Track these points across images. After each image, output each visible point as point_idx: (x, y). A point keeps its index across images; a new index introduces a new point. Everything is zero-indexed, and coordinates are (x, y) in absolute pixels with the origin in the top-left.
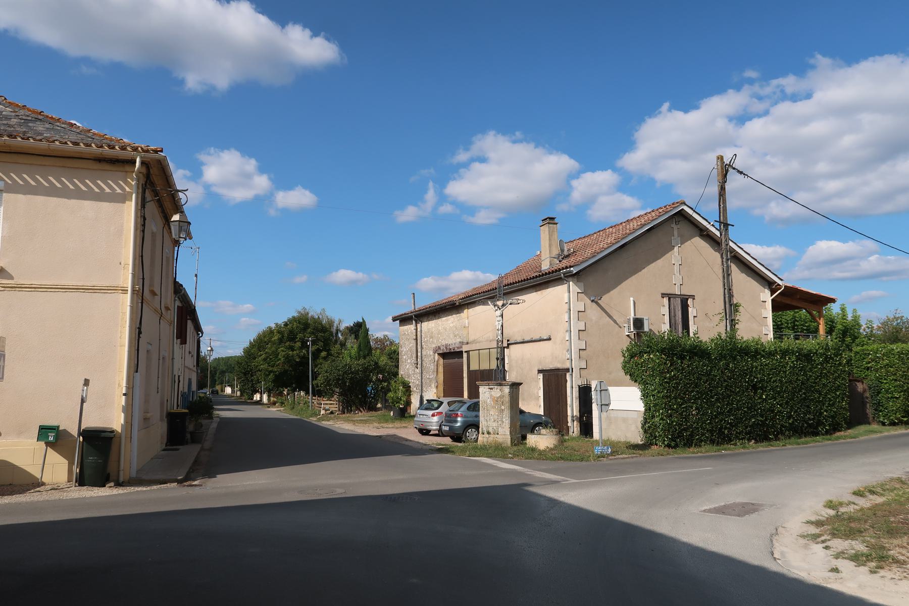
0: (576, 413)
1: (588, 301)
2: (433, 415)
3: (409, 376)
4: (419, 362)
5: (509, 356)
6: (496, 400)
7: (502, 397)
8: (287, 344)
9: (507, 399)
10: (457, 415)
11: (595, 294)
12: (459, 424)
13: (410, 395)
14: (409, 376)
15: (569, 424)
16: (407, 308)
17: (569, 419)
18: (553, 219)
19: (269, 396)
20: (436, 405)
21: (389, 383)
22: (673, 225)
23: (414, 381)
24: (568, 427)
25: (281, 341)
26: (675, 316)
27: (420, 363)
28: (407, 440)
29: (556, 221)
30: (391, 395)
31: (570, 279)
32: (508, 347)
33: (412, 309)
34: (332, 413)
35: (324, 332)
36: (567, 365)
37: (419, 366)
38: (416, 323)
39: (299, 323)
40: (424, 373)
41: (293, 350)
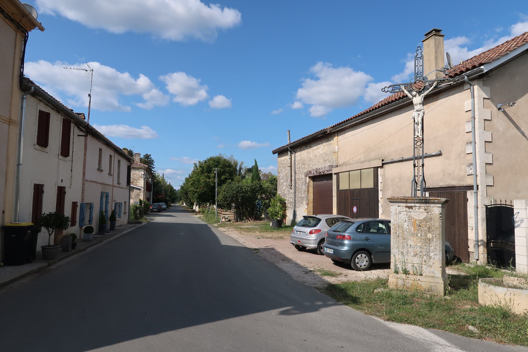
0: (482, 236)
1: (495, 109)
2: (311, 233)
3: (285, 195)
5: (383, 176)
8: (206, 174)
9: (437, 223)
11: (503, 100)
12: (346, 248)
13: (286, 210)
14: (285, 195)
15: (471, 249)
16: (285, 142)
18: (439, 31)
19: (199, 207)
21: (270, 201)
23: (289, 199)
24: (468, 253)
25: (202, 172)
27: (293, 185)
29: (441, 33)
30: (270, 209)
31: (476, 82)
32: (382, 167)
33: (288, 143)
34: (229, 221)
35: (230, 168)
36: (469, 181)
38: (291, 154)
39: (214, 161)
40: (297, 193)
41: (209, 178)
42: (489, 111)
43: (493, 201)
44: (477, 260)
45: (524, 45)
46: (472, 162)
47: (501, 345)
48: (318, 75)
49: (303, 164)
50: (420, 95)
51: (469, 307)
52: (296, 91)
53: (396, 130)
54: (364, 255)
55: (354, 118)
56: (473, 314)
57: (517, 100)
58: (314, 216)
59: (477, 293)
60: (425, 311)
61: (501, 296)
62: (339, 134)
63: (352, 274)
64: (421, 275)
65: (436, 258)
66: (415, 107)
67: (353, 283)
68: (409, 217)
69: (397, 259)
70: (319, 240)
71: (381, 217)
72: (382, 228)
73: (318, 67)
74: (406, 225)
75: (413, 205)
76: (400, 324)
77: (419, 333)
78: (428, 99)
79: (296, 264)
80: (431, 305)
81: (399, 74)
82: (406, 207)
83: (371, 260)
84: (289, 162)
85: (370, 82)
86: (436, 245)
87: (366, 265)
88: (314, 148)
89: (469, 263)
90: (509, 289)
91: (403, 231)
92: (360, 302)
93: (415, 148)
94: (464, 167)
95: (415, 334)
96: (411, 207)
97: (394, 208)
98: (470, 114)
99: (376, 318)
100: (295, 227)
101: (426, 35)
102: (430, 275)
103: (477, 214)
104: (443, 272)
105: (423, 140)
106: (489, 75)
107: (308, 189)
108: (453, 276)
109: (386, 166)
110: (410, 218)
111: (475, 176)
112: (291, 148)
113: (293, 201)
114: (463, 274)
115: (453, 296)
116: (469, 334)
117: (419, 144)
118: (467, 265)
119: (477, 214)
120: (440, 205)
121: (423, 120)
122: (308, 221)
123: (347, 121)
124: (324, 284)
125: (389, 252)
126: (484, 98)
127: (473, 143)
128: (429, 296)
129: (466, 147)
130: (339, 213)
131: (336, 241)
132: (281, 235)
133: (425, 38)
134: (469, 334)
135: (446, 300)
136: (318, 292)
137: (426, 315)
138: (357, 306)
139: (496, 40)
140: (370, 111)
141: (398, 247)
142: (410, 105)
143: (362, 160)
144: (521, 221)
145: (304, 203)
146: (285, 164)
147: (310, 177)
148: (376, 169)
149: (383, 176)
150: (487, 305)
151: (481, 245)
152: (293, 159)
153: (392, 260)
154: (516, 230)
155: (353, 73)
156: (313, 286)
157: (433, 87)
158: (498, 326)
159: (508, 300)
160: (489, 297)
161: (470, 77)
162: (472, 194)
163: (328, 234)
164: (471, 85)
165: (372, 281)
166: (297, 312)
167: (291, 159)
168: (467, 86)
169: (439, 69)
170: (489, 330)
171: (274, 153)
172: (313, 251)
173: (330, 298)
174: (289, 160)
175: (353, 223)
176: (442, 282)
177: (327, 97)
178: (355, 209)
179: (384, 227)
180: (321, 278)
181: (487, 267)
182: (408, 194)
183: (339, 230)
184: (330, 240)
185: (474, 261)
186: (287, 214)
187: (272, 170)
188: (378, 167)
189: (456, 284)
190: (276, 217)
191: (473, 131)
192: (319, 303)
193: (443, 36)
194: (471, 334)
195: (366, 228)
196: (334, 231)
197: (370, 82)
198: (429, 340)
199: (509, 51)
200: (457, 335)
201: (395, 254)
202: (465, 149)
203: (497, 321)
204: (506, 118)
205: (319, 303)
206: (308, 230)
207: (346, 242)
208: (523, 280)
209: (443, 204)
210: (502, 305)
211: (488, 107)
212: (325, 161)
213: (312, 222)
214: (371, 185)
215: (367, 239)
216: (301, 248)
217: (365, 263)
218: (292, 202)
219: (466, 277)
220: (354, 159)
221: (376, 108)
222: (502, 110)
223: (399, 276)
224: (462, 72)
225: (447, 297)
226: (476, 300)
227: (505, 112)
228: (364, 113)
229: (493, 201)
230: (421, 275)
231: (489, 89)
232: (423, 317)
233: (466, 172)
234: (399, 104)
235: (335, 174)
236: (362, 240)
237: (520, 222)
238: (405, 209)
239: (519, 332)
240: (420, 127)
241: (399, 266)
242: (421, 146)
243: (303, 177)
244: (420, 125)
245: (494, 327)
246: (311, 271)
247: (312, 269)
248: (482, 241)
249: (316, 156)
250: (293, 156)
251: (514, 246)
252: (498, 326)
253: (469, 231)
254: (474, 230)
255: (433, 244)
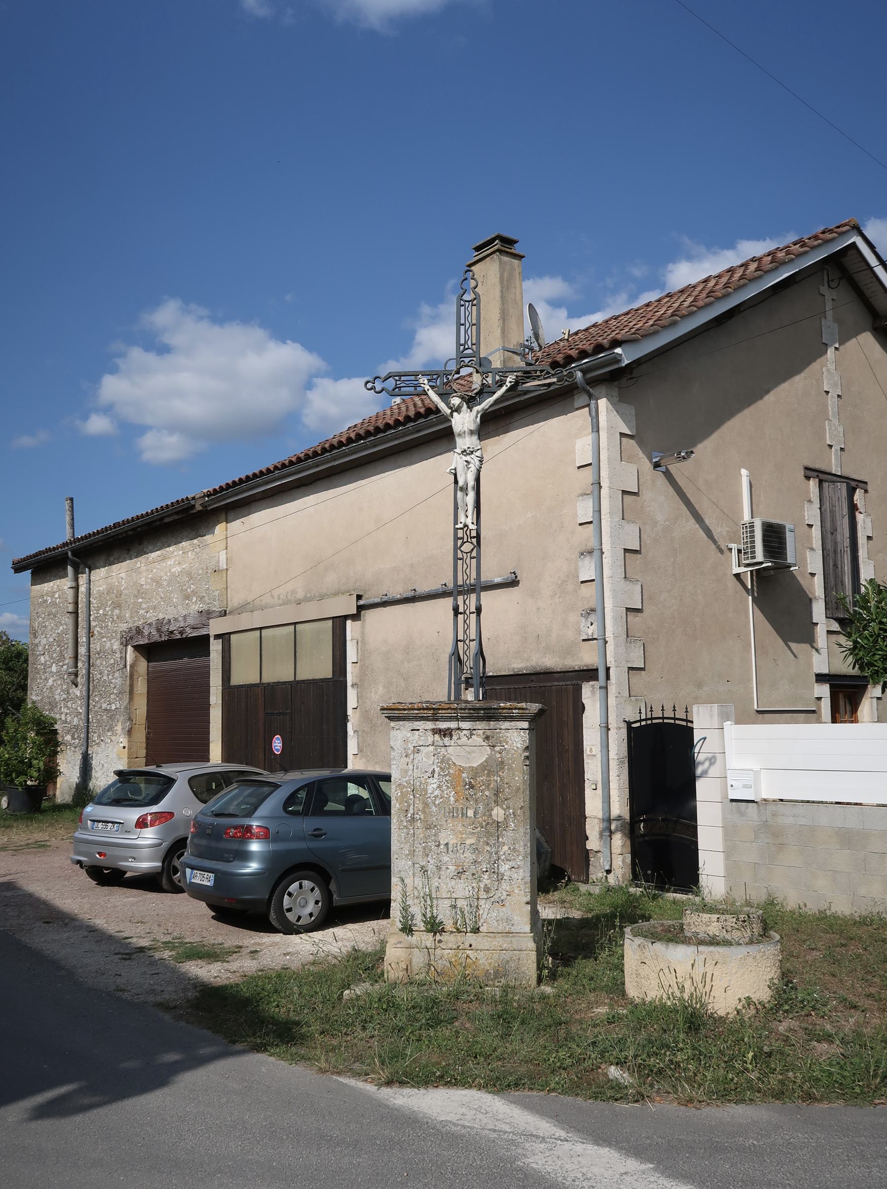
0: (620, 807)
1: (647, 466)
2: (141, 824)
3: (53, 705)
4: (81, 670)
6: (469, 784)
7: (493, 767)
9: (518, 776)
10: (247, 833)
11: (665, 440)
12: (253, 866)
13: (55, 753)
15: (593, 843)
16: (56, 535)
17: (593, 829)
18: (508, 242)
20: (153, 790)
22: (824, 289)
23: (66, 717)
24: (586, 855)
26: (834, 532)
27: (83, 671)
28: (49, 550)
29: (517, 249)
31: (602, 389)
32: (356, 617)
33: (67, 537)
36: (587, 658)
37: (81, 680)
42: (633, 469)
43: (643, 711)
44: (609, 872)
45: (710, 304)
46: (592, 604)
47: (690, 1112)
48: (167, 339)
49: (117, 605)
50: (470, 408)
51: (603, 1010)
52: (96, 380)
53: (404, 502)
54: (307, 884)
55: (276, 468)
56: (618, 1031)
57: (695, 445)
58: (152, 768)
59: (620, 968)
60: (488, 1039)
61: (683, 970)
62: (231, 515)
63: (275, 944)
64: (476, 930)
65: (515, 876)
66: (459, 441)
67: (279, 976)
68: (442, 761)
69: (409, 889)
70: (166, 845)
71: (354, 764)
72: (357, 798)
73: (166, 315)
74: (432, 785)
75: (453, 725)
76: (422, 1091)
77: (478, 1110)
78: (493, 423)
79: (93, 930)
80: (506, 1016)
81: (398, 361)
82: (435, 731)
83: (327, 895)
84: (71, 599)
85: (318, 374)
86: (515, 841)
87: (315, 914)
88: (153, 555)
89: (586, 881)
90: (702, 948)
91: (426, 805)
92: (303, 1037)
93: (456, 559)
94: (573, 617)
95: (470, 1115)
96: (446, 733)
97: (401, 735)
98: (588, 475)
99: (352, 1082)
100: (89, 809)
101: (478, 249)
102: (500, 928)
103: (606, 746)
104: (534, 913)
105: (478, 537)
106: (635, 373)
107: (132, 686)
108: (561, 924)
109: (368, 615)
110: (445, 762)
111: (601, 642)
112: (75, 553)
113: (82, 724)
114: (576, 914)
115: (561, 981)
116: (610, 1093)
117: (467, 547)
118: (583, 888)
119: (606, 746)
120: (525, 725)
121: (478, 480)
122: (132, 788)
123: (255, 475)
124: (185, 990)
125: (386, 868)
126: (622, 435)
127: (597, 553)
128: (498, 993)
129: (580, 564)
130: (228, 756)
131: (222, 845)
132: (38, 836)
133: (474, 256)
134: (610, 1093)
135: (544, 997)
136: (167, 1017)
137: (495, 1050)
138: (293, 1050)
139: (633, 297)
140: (324, 450)
141: (412, 853)
142: (445, 437)
143: (300, 595)
144: (710, 760)
145: (119, 728)
146: (54, 604)
147: (137, 648)
148: (339, 623)
149: (361, 643)
150: (648, 999)
151: (617, 830)
152: (83, 589)
153: (396, 894)
154: (700, 785)
155: (272, 345)
156: (151, 998)
157: (504, 388)
158: (680, 1057)
159: (698, 978)
160: (653, 976)
161: (589, 376)
162: (593, 692)
163: (198, 824)
164: (590, 396)
165: (334, 961)
166: (96, 1099)
167: (76, 588)
168: (581, 399)
169: (511, 347)
170: (660, 1072)
171: (19, 567)
172: (148, 883)
173: (209, 1033)
174: (70, 594)
175: (276, 786)
176: (532, 945)
177: (193, 410)
178: (277, 744)
179: (365, 794)
180: (174, 971)
181: (632, 890)
182: (440, 692)
183: (231, 811)
184: (204, 842)
185: (601, 874)
186: (62, 768)
187: (13, 625)
188: (346, 617)
189: (571, 946)
190: (21, 779)
191: (596, 522)
192: (172, 1057)
193: (520, 257)
194: (617, 1092)
195: (313, 800)
196: (217, 815)
197: (318, 374)
198: (507, 1128)
199: (678, 316)
200: (580, 1099)
201: (403, 875)
202: (577, 570)
203: (676, 1042)
204: (671, 489)
205: (172, 1057)
206: (133, 814)
207: (255, 847)
208: (731, 920)
209: (535, 720)
210: (686, 996)
211: (630, 459)
212: (187, 597)
213: (146, 789)
214: (323, 670)
215: (317, 834)
216: (108, 876)
217: (311, 907)
218: (76, 727)
219: (584, 923)
220: (276, 593)
221: (341, 444)
222: (663, 469)
223: (414, 939)
224: (569, 359)
225: (548, 989)
226: (618, 988)
227: (668, 475)
228: (307, 457)
229: (643, 711)
230: (476, 930)
231: (633, 412)
232: (487, 1057)
233: (579, 632)
234: (405, 435)
235: (217, 637)
236: (303, 839)
237: (707, 764)
238: (430, 738)
239: (729, 1067)
240: (471, 498)
241: (416, 910)
242: (474, 554)
243: (116, 646)
244: (471, 495)
245: (671, 1061)
246: (142, 949)
247: (144, 943)
248: (619, 818)
249: (157, 582)
250: (83, 579)
251: (695, 828)
252: (680, 1057)
253: (588, 792)
254: (599, 791)
255: (507, 837)
